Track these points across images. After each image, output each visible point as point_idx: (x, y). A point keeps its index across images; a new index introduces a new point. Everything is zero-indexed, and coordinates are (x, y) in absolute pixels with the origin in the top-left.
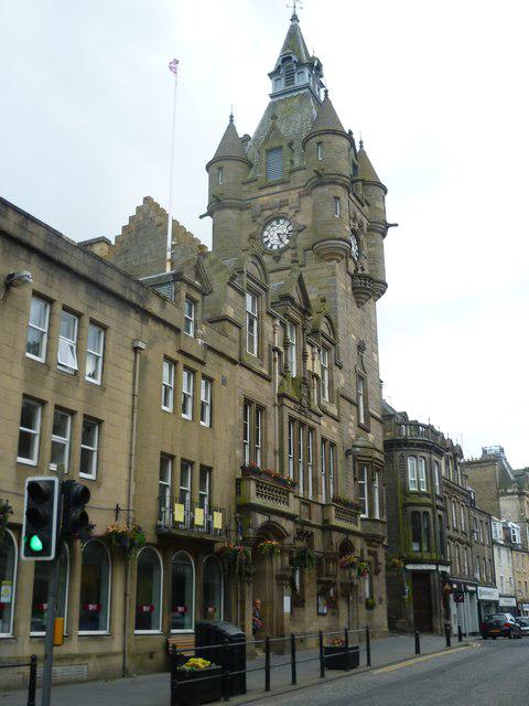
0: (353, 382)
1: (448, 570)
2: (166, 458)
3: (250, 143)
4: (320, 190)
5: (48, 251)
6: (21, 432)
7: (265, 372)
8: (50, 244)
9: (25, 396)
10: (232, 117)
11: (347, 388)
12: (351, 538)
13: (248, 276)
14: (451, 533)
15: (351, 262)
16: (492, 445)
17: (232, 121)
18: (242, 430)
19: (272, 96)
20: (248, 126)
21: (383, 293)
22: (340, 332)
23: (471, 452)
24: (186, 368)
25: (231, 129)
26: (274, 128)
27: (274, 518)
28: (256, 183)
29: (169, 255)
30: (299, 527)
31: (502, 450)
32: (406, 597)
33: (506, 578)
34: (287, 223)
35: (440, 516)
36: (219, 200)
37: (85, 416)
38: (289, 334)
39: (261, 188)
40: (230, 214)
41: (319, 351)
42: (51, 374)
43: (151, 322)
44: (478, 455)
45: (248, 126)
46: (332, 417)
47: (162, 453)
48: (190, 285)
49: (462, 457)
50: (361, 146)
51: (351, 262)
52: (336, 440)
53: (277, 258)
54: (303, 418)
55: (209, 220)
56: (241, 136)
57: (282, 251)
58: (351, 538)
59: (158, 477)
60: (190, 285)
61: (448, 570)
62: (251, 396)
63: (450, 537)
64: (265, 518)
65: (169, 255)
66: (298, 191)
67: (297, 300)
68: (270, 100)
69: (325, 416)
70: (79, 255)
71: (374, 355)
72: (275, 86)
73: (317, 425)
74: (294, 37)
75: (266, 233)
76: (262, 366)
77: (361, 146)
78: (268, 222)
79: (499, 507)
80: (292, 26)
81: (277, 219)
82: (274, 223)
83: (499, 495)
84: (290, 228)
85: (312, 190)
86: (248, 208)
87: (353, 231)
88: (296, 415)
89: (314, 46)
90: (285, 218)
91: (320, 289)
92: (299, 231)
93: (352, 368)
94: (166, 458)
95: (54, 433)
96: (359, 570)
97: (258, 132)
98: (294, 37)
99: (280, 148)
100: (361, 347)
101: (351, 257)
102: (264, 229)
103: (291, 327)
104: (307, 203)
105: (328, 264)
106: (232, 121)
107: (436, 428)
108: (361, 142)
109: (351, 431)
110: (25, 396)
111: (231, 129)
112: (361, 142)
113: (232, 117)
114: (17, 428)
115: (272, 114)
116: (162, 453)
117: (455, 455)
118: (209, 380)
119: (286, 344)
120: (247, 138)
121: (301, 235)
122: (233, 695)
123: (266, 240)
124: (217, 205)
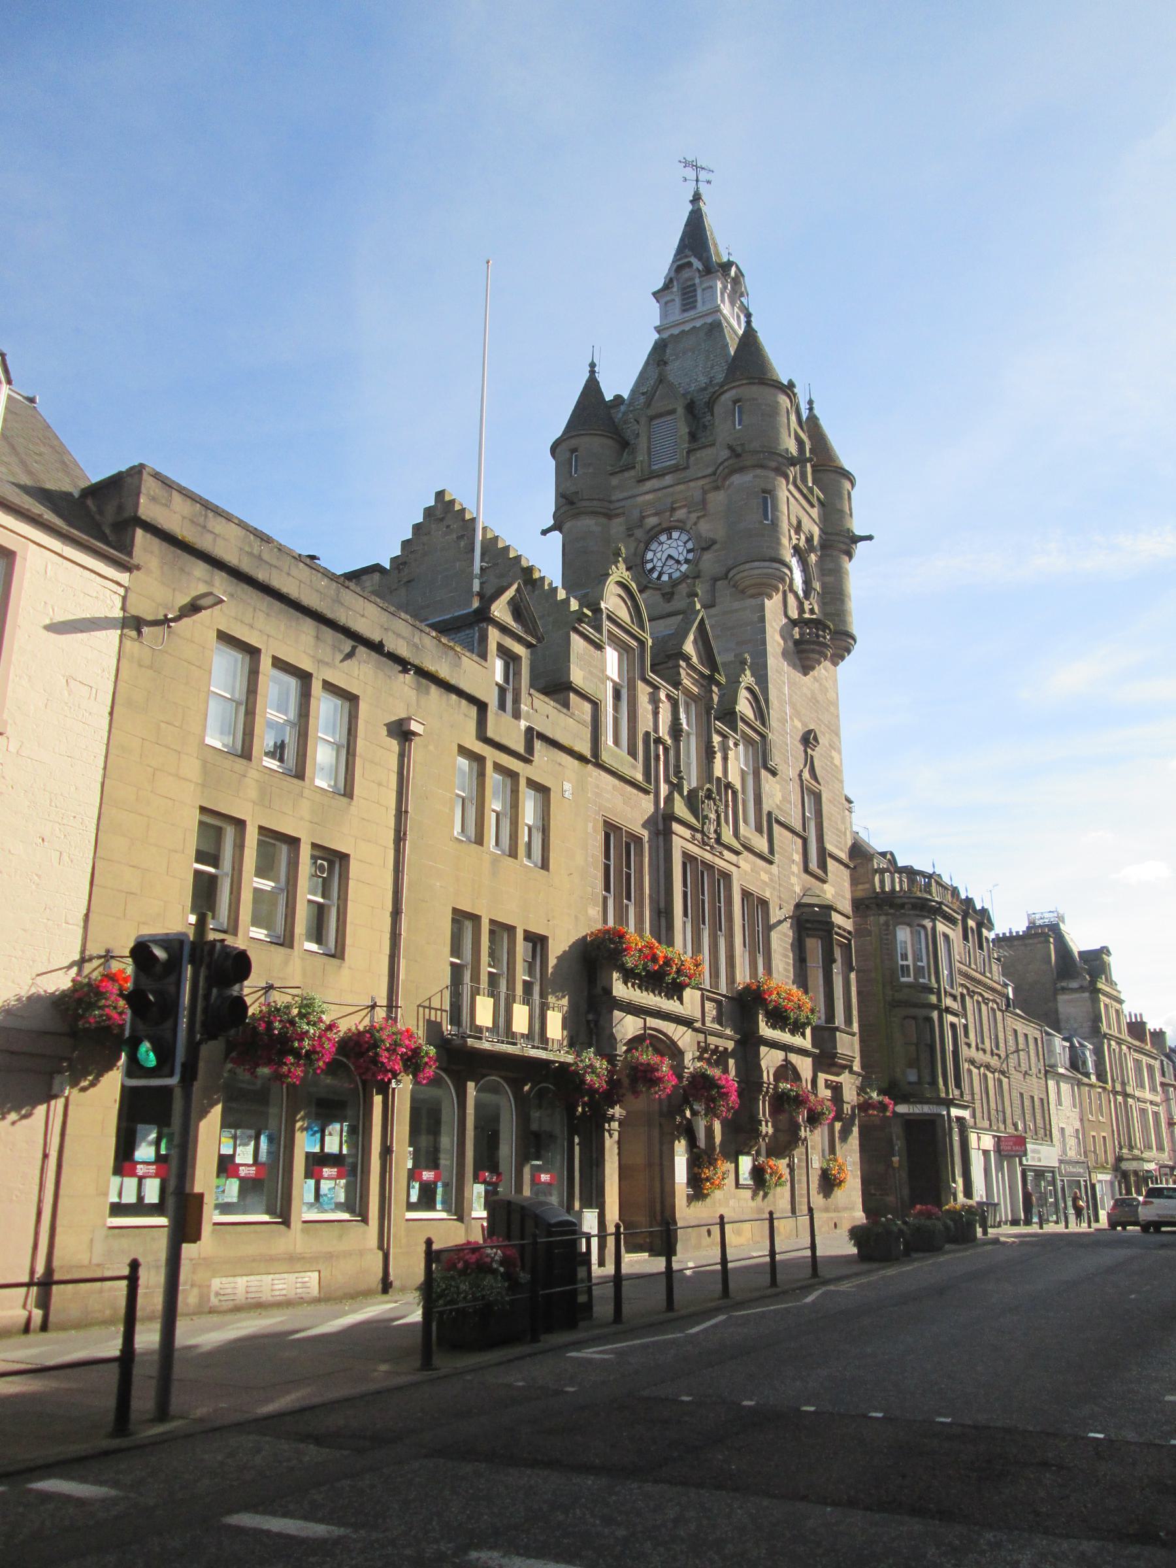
0: (795, 797)
1: (965, 1114)
2: (461, 918)
3: (623, 408)
4: (737, 479)
5: (246, 566)
6: (197, 873)
7: (639, 777)
8: (250, 554)
9: (203, 809)
10: (592, 365)
11: (786, 807)
12: (794, 1058)
13: (609, 618)
14: (972, 1053)
15: (791, 599)
16: (1043, 912)
17: (592, 372)
18: (600, 875)
19: (658, 330)
20: (618, 382)
21: (849, 651)
22: (774, 715)
23: (1008, 920)
24: (498, 768)
25: (592, 388)
26: (661, 380)
27: (652, 1022)
28: (632, 473)
29: (476, 586)
30: (701, 1037)
31: (1061, 918)
32: (896, 1159)
33: (1069, 1131)
34: (684, 537)
35: (953, 1026)
36: (572, 503)
37: (314, 846)
38: (683, 716)
39: (641, 481)
40: (588, 523)
41: (736, 745)
42: (253, 774)
43: (434, 690)
44: (1020, 927)
45: (618, 382)
46: (760, 856)
47: (455, 910)
48: (504, 629)
49: (990, 928)
50: (811, 409)
51: (791, 599)
52: (767, 894)
53: (668, 596)
54: (708, 856)
55: (557, 536)
56: (608, 397)
57: (674, 583)
58: (794, 1058)
59: (448, 949)
60: (504, 629)
61: (965, 1114)
62: (618, 820)
63: (972, 1062)
64: (639, 1022)
65: (476, 586)
66: (701, 482)
67: (695, 660)
68: (657, 336)
69: (746, 853)
70: (302, 572)
71: (834, 754)
72: (664, 314)
73: (733, 869)
74: (695, 237)
75: (649, 555)
76: (634, 767)
77: (811, 409)
78: (652, 536)
79: (1056, 1011)
80: (692, 212)
81: (668, 530)
82: (663, 538)
83: (1056, 992)
84: (690, 545)
85: (725, 479)
86: (618, 515)
87: (796, 549)
88: (695, 850)
89: (724, 241)
90: (682, 530)
91: (1049, 1071)
92: (704, 549)
93: (792, 773)
94: (461, 918)
95: (257, 875)
96: (810, 1111)
97: (633, 391)
98: (695, 237)
99: (673, 412)
100: (808, 739)
101: (792, 590)
102: (647, 548)
103: (687, 705)
104: (717, 499)
105: (753, 602)
106: (592, 372)
107: (946, 879)
108: (811, 402)
109: (794, 880)
110: (203, 809)
111: (592, 388)
112: (811, 402)
113: (592, 365)
114: (188, 866)
115: (659, 354)
116: (455, 910)
117: (980, 925)
118: (542, 790)
119: (676, 731)
120: (618, 398)
121: (707, 556)
122: (549, 1330)
123: (649, 566)
124: (569, 508)
